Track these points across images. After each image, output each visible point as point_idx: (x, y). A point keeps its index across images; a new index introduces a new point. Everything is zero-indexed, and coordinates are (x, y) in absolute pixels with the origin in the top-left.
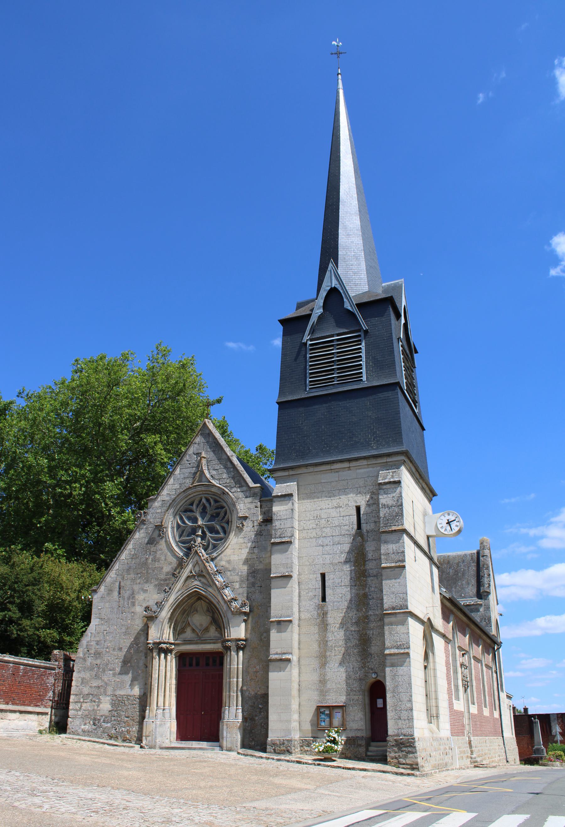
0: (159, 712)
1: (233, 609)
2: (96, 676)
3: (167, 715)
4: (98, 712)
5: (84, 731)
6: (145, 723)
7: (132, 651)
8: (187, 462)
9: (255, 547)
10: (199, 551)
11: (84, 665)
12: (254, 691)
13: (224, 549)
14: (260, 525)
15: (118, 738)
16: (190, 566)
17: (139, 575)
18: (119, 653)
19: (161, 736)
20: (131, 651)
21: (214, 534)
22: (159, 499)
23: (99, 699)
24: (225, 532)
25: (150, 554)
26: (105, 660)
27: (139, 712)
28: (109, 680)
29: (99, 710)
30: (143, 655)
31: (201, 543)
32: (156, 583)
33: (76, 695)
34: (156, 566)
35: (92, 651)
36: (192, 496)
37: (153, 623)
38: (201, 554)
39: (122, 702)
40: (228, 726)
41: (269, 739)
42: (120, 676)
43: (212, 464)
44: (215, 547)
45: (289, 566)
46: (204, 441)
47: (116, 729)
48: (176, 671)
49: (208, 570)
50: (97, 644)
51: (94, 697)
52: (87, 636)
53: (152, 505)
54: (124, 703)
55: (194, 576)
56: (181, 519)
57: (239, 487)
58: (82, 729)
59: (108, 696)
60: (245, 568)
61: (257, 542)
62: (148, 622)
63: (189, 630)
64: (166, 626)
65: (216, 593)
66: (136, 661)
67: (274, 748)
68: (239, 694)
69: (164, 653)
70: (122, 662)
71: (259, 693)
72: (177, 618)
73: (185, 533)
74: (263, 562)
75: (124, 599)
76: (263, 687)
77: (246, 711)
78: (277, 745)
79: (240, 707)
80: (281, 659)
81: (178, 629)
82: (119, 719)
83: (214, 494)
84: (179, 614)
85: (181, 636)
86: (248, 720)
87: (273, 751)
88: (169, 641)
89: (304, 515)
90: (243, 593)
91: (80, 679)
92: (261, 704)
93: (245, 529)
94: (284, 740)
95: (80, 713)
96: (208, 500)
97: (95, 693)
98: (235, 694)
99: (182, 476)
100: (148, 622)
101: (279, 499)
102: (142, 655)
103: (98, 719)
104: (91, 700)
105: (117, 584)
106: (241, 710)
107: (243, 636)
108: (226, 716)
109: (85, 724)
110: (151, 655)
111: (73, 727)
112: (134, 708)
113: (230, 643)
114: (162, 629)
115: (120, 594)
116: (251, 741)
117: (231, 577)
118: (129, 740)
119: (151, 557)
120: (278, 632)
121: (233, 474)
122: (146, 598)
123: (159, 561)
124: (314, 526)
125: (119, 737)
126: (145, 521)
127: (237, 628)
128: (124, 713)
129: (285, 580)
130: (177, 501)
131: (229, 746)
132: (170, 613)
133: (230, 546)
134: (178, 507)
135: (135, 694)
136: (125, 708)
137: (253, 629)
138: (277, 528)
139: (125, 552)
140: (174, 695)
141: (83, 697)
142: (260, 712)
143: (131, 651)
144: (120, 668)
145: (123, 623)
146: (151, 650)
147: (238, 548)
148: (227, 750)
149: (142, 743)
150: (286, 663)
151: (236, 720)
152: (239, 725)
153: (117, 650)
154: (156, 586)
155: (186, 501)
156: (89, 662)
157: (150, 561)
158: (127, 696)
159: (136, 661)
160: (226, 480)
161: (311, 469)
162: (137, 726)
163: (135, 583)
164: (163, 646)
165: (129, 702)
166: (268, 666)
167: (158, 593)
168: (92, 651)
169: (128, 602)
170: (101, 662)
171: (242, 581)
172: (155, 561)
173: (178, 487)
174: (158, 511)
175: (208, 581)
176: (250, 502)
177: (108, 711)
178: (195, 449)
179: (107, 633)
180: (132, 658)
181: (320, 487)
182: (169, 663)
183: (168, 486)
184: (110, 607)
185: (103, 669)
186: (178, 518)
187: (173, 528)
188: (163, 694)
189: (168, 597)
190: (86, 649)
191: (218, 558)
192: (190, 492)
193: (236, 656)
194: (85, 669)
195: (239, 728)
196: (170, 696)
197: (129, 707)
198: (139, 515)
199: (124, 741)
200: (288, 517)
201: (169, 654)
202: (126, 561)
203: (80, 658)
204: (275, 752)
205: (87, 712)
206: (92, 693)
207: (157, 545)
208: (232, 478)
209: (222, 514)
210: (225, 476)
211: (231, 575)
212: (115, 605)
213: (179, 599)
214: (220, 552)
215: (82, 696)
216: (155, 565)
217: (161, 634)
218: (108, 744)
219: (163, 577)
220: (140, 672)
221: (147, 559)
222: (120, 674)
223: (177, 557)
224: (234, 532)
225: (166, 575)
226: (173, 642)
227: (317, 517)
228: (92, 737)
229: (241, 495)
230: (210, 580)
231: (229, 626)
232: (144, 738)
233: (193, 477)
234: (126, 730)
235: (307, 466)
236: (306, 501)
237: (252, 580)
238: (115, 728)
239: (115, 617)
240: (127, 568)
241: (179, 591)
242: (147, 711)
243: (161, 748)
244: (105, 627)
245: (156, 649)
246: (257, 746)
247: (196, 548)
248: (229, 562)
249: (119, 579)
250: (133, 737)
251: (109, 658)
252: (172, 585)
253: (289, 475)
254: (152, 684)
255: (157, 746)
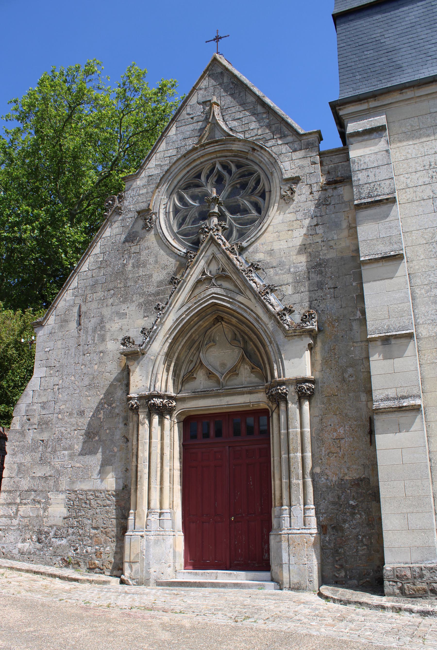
0: (152, 519)
1: (287, 327)
2: (41, 459)
3: (168, 525)
4: (45, 520)
5: (22, 553)
6: (127, 539)
7: (101, 416)
8: (188, 117)
9: (317, 225)
10: (216, 237)
11: (22, 443)
12: (336, 474)
13: (260, 233)
14: (323, 189)
15: (79, 566)
16: (202, 263)
17: (112, 292)
18: (79, 420)
19: (159, 561)
20: (100, 416)
21: (238, 214)
22: (143, 175)
23: (48, 498)
24: (259, 211)
25: (130, 257)
26: (57, 433)
27: (116, 519)
28: (63, 466)
29: (47, 517)
30: (121, 420)
31: (220, 225)
32: (141, 300)
33: (9, 492)
34: (141, 274)
35: (35, 420)
36: (198, 162)
37: (138, 364)
38: (220, 242)
39: (86, 503)
40: (291, 542)
41: (388, 567)
42: (81, 457)
43: (230, 112)
44: (242, 235)
45: (394, 239)
46: (215, 83)
47: (77, 549)
48: (180, 446)
49: (234, 265)
50: (43, 408)
51: (38, 495)
52: (26, 395)
53: (131, 186)
54: (90, 504)
55: (209, 279)
56: (181, 199)
57: (280, 138)
58: (20, 549)
59: (62, 492)
60: (303, 259)
61: (321, 216)
62: (129, 363)
63: (201, 375)
64: (161, 368)
65: (253, 304)
66: (108, 431)
67: (400, 585)
68: (309, 480)
69: (158, 414)
70: (85, 434)
71: (347, 478)
72: (179, 354)
73: (188, 220)
74: (334, 247)
75: (87, 332)
76: (355, 467)
77: (324, 513)
78: (408, 579)
79: (313, 506)
80: (400, 407)
81: (182, 375)
82: (81, 532)
83: (237, 154)
84: (183, 347)
85: (187, 386)
86: (330, 529)
87: (398, 591)
88: (166, 393)
89: (405, 165)
90: (301, 302)
91: (15, 466)
92: (354, 498)
93: (296, 197)
94: (421, 569)
95: (15, 522)
96: (225, 167)
97: (40, 488)
98: (301, 482)
99: (181, 137)
100: (129, 363)
101: (360, 138)
102: (119, 420)
103: (46, 532)
104: (34, 500)
105: (76, 309)
106: (314, 511)
107: (308, 374)
108: (286, 523)
109: (24, 541)
110: (135, 419)
111: (5, 546)
112: (107, 512)
113: (284, 387)
114: (155, 372)
115: (80, 324)
116: (339, 570)
117: (277, 278)
118: (99, 568)
119: (131, 261)
120: (385, 358)
121: (268, 121)
122: (124, 327)
123: (144, 266)
124: (427, 180)
125: (82, 564)
126: (120, 208)
127: (296, 360)
128: (90, 522)
129: (388, 266)
130: (174, 173)
131: (295, 580)
132: (167, 344)
133: (270, 228)
134: (175, 182)
135: (109, 488)
136: (91, 512)
137: (325, 362)
138: (361, 182)
139: (88, 260)
140: (178, 488)
141: (20, 495)
142: (353, 514)
143: (100, 416)
144: (81, 445)
145: (85, 371)
146: (135, 410)
147: (287, 228)
148: (291, 589)
149: (123, 574)
150: (410, 414)
151: (304, 531)
152: (313, 539)
153: (75, 416)
154: (140, 305)
155: (188, 172)
156: (31, 438)
157: (129, 267)
158: (94, 491)
159: (108, 431)
160: (255, 131)
161: (409, 94)
162: (114, 544)
163: (105, 305)
164: (158, 401)
165: (98, 501)
166: (371, 421)
167: (145, 317)
168: (35, 420)
169: (94, 337)
170: (50, 437)
171: (297, 282)
172: (138, 267)
173: (175, 153)
174: (141, 192)
175: (236, 286)
176: (300, 157)
177: (61, 519)
178: (200, 96)
179: (59, 389)
180: (101, 426)
181: (429, 120)
182: (167, 432)
183: (158, 155)
184: (63, 346)
185: (52, 448)
186: (175, 198)
187: (167, 214)
188: (158, 487)
189: (164, 317)
190: (25, 417)
191: (251, 249)
192: (195, 156)
193: (298, 411)
194: (23, 449)
195: (314, 545)
196: (172, 490)
197: (98, 511)
198: (110, 202)
199: (91, 569)
200: (380, 163)
201: (168, 417)
202: (90, 274)
203: (17, 431)
204: (403, 592)
205: (26, 520)
206: (35, 488)
207: (141, 243)
208: (267, 126)
209: (252, 183)
210: (253, 125)
211: (276, 274)
212: (72, 343)
213: (183, 319)
214: (253, 239)
215: (18, 493)
216: (138, 273)
217: (153, 381)
218: (61, 578)
219: (152, 289)
220: (116, 449)
221: (124, 265)
222: (81, 454)
223: (177, 256)
224: (276, 205)
225: (158, 287)
226: (173, 394)
227: (430, 165)
228: (36, 563)
229: (285, 149)
230: (239, 282)
231: (281, 358)
232: (126, 565)
233: (199, 134)
234: (94, 550)
235: (402, 90)
236: (405, 143)
237: (317, 278)
238: (74, 546)
239: (72, 361)
240: (91, 283)
241: (182, 306)
242: (131, 517)
243: (159, 584)
244: (55, 380)
245: (144, 408)
246: (351, 579)
247: (211, 232)
248: (271, 252)
249: (78, 301)
250: (106, 563)
251: (63, 429)
252: (171, 296)
253: (368, 109)
254: (139, 469)
255: (152, 581)
